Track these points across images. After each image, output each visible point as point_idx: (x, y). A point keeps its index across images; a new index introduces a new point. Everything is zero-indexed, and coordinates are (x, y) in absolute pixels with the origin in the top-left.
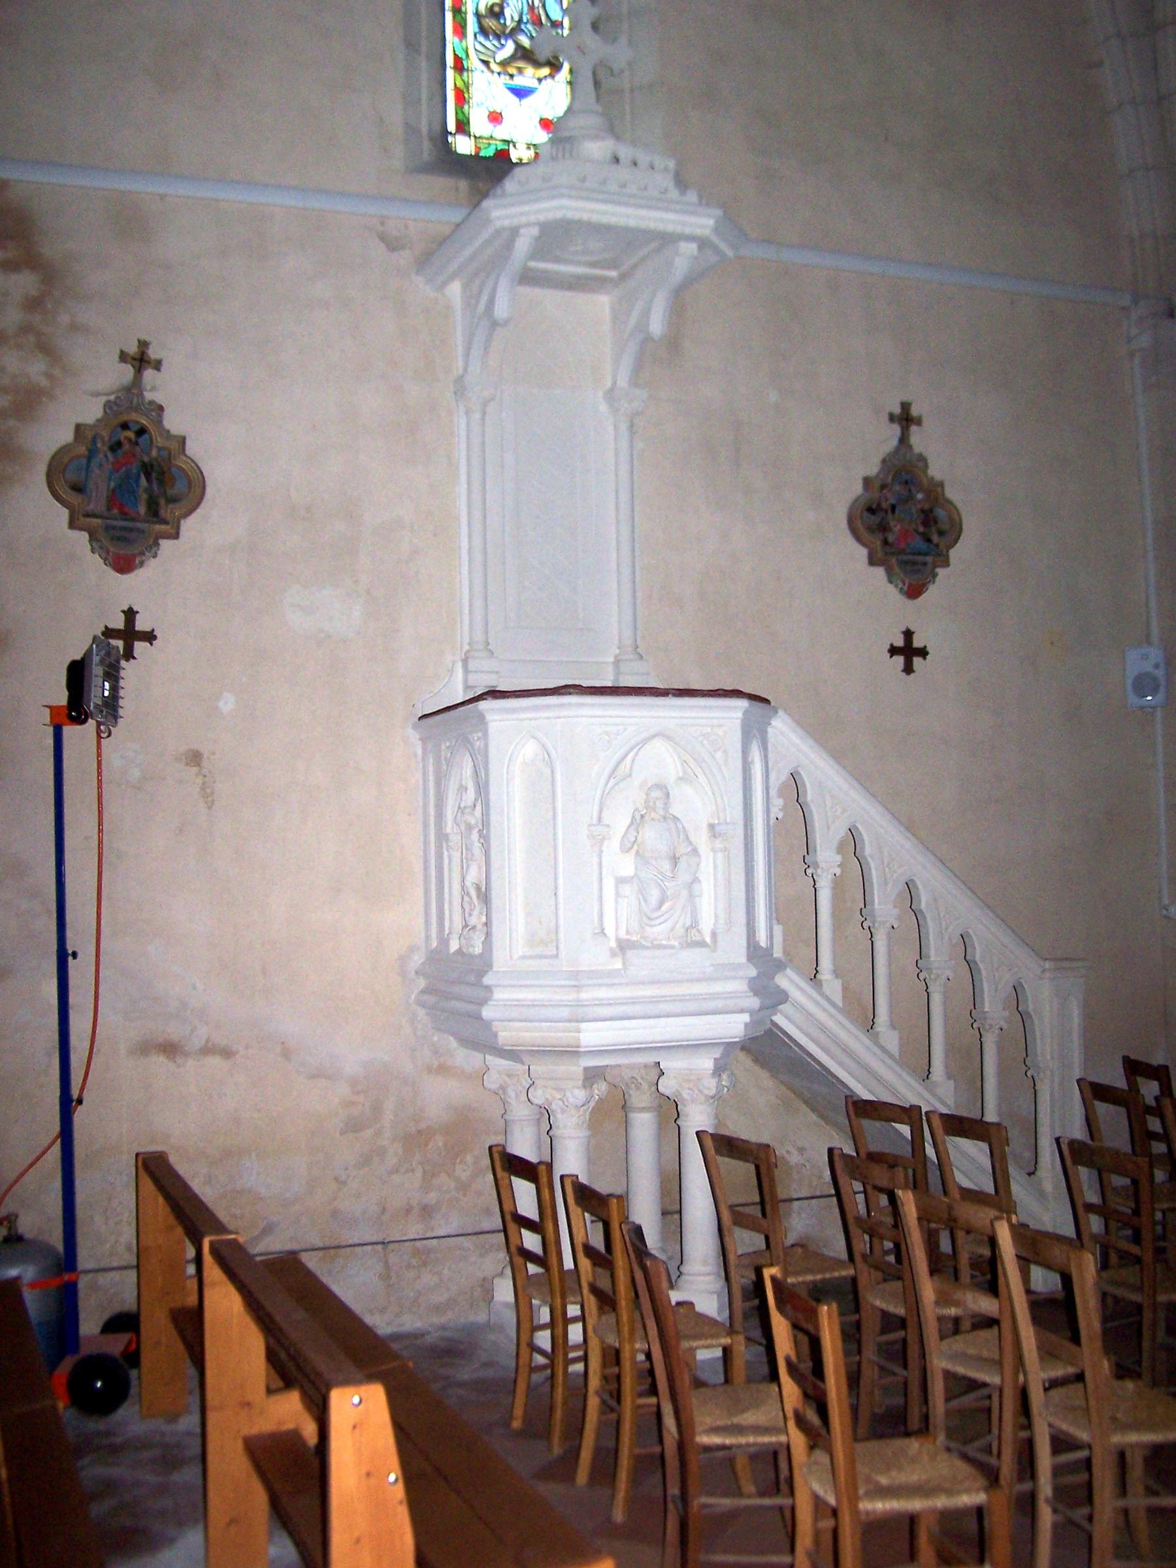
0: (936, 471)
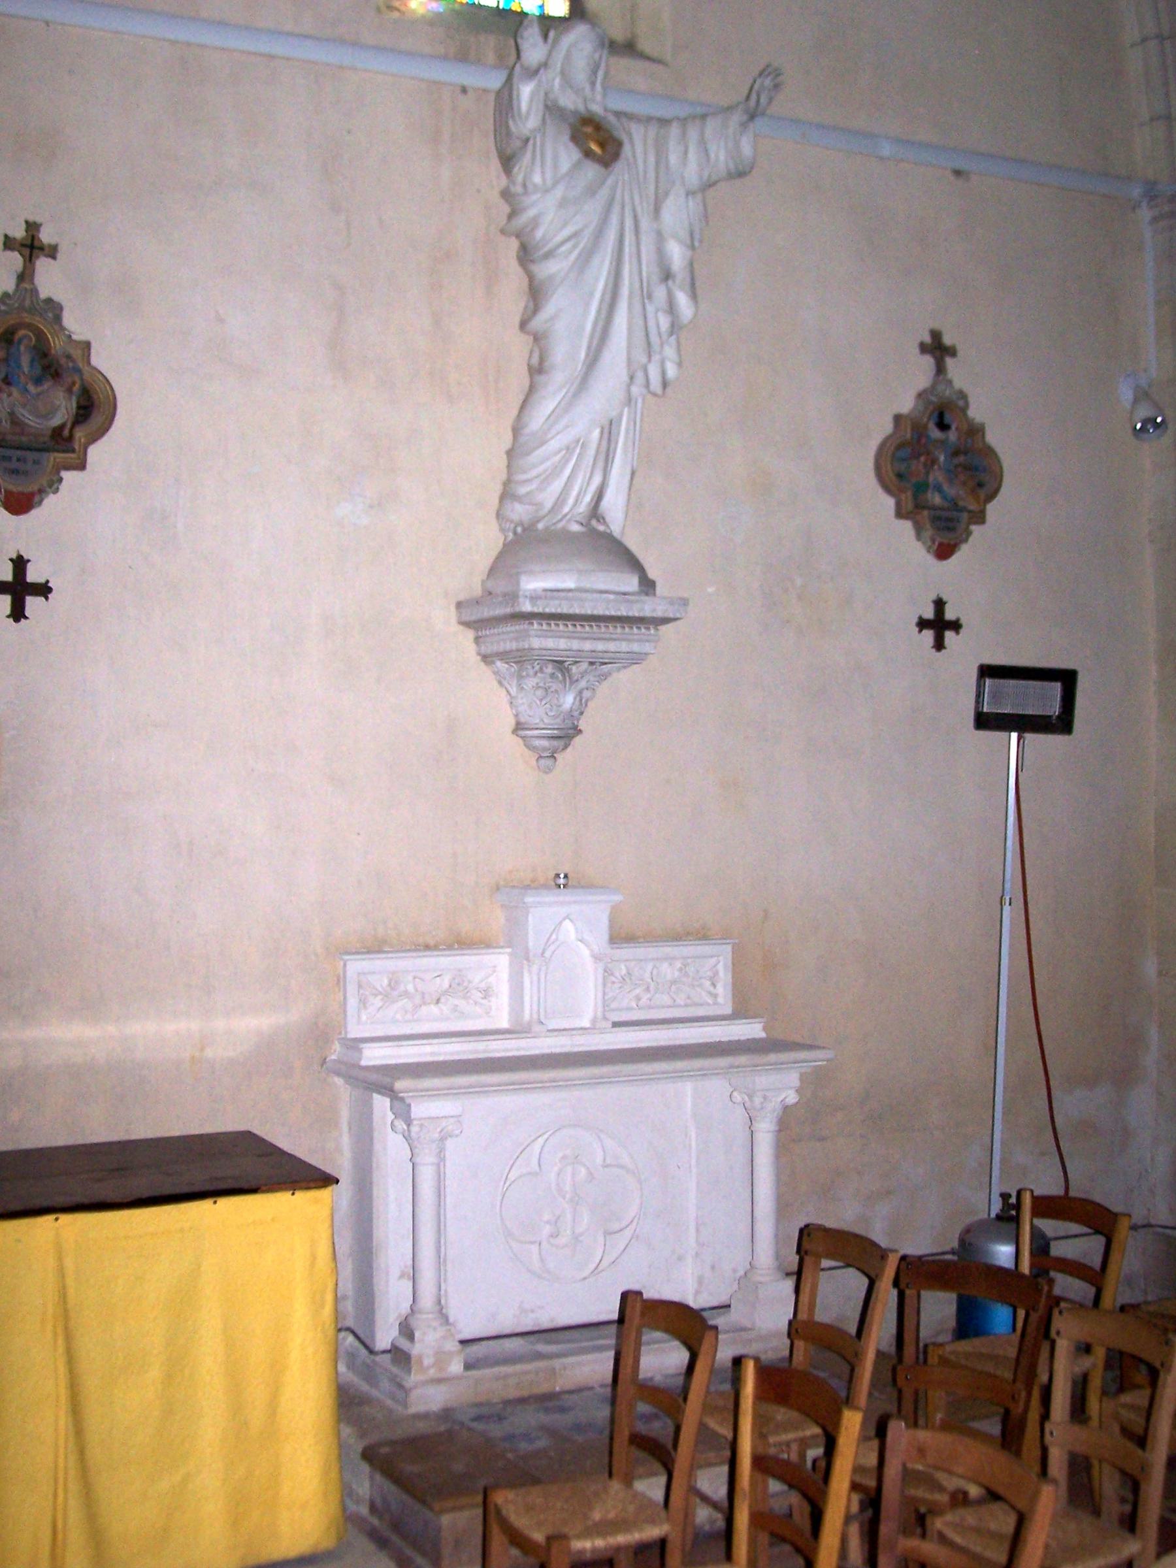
0: (976, 413)
